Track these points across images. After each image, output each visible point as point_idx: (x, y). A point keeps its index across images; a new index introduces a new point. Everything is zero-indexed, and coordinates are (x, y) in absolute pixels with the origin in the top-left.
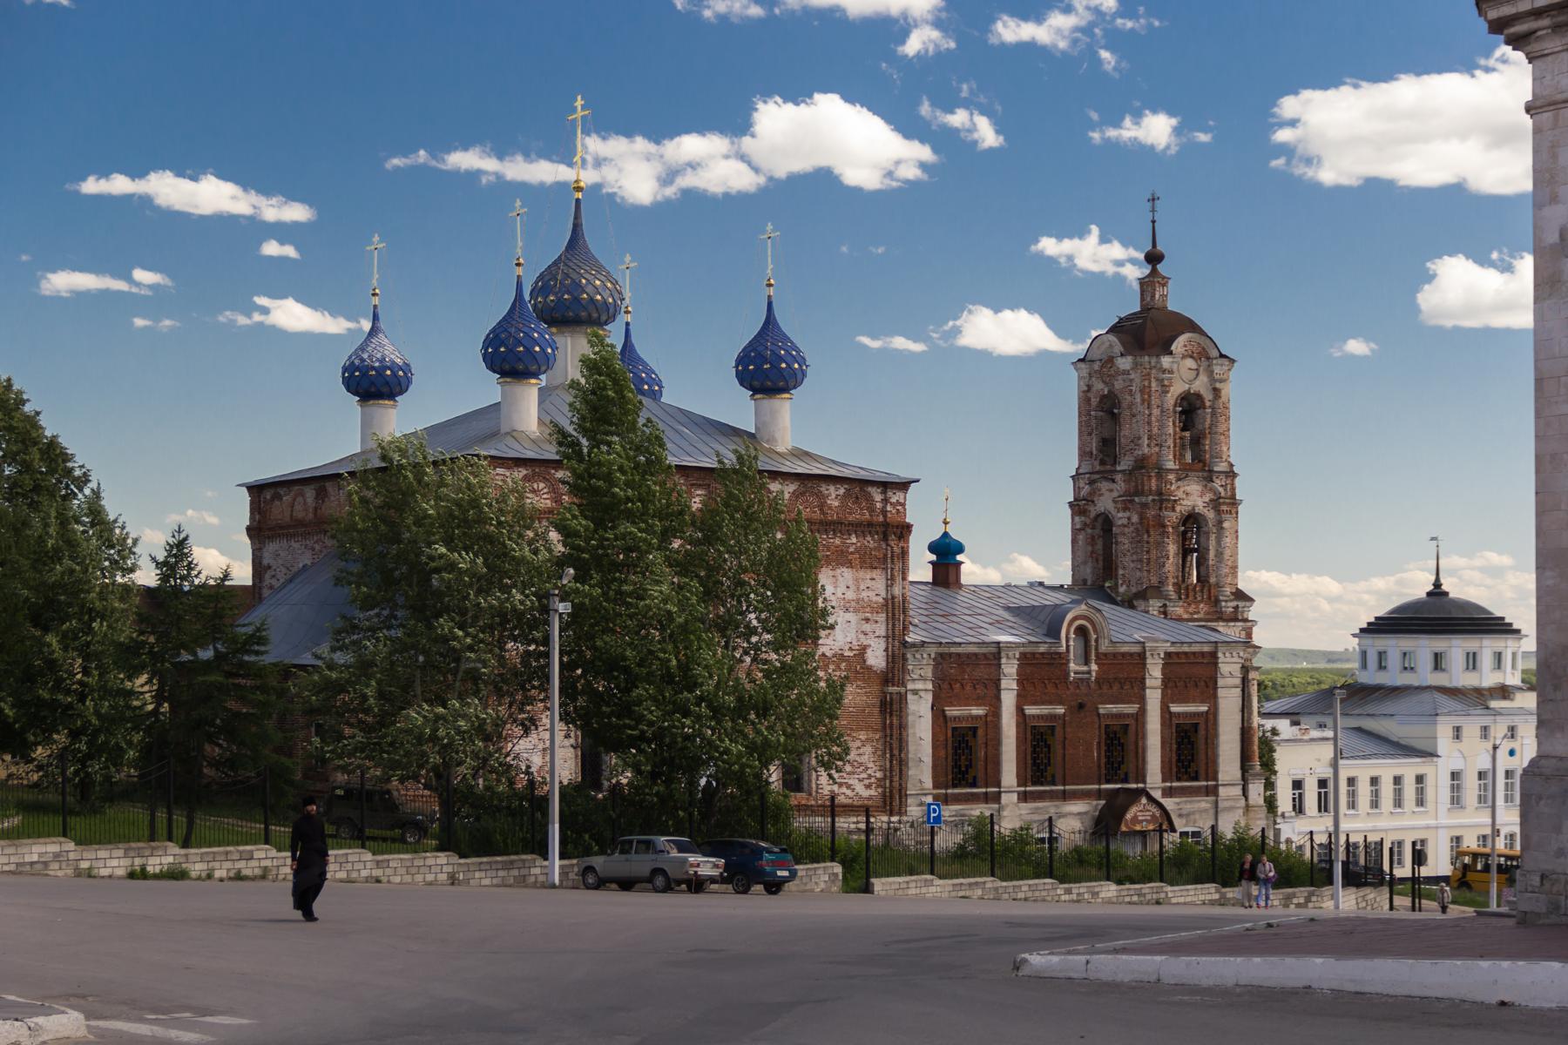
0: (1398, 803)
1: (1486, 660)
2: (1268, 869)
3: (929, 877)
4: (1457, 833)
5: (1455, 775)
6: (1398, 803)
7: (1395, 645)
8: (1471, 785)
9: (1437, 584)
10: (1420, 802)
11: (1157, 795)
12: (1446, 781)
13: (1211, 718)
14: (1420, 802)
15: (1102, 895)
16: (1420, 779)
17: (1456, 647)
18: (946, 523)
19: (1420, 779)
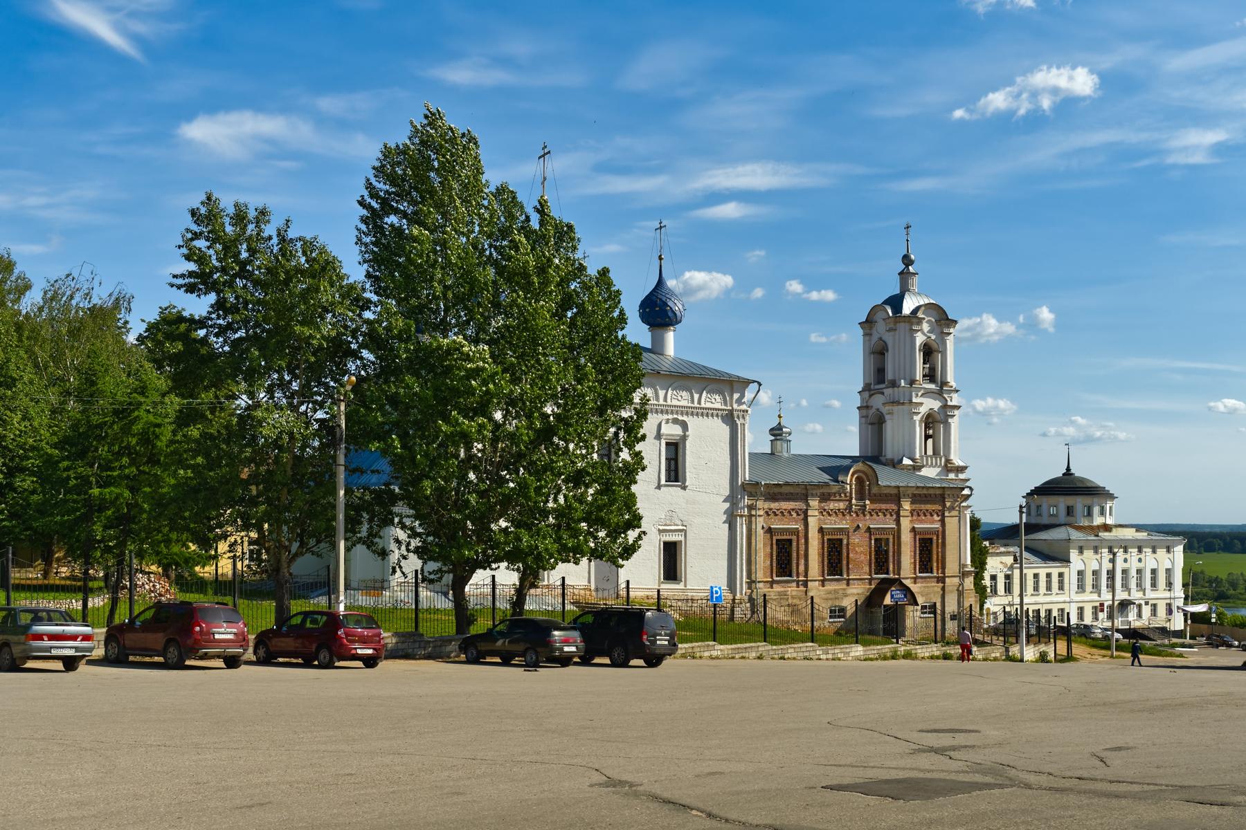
0: (1049, 588)
1: (1096, 510)
2: (567, 641)
3: (711, 643)
4: (1081, 605)
5: (1080, 573)
6: (1049, 588)
7: (1045, 501)
8: (1055, 584)
9: (1068, 469)
10: (1061, 588)
11: (907, 582)
12: (1074, 577)
14: (1061, 588)
15: (852, 654)
16: (1061, 575)
17: (1079, 502)
19: (1061, 575)
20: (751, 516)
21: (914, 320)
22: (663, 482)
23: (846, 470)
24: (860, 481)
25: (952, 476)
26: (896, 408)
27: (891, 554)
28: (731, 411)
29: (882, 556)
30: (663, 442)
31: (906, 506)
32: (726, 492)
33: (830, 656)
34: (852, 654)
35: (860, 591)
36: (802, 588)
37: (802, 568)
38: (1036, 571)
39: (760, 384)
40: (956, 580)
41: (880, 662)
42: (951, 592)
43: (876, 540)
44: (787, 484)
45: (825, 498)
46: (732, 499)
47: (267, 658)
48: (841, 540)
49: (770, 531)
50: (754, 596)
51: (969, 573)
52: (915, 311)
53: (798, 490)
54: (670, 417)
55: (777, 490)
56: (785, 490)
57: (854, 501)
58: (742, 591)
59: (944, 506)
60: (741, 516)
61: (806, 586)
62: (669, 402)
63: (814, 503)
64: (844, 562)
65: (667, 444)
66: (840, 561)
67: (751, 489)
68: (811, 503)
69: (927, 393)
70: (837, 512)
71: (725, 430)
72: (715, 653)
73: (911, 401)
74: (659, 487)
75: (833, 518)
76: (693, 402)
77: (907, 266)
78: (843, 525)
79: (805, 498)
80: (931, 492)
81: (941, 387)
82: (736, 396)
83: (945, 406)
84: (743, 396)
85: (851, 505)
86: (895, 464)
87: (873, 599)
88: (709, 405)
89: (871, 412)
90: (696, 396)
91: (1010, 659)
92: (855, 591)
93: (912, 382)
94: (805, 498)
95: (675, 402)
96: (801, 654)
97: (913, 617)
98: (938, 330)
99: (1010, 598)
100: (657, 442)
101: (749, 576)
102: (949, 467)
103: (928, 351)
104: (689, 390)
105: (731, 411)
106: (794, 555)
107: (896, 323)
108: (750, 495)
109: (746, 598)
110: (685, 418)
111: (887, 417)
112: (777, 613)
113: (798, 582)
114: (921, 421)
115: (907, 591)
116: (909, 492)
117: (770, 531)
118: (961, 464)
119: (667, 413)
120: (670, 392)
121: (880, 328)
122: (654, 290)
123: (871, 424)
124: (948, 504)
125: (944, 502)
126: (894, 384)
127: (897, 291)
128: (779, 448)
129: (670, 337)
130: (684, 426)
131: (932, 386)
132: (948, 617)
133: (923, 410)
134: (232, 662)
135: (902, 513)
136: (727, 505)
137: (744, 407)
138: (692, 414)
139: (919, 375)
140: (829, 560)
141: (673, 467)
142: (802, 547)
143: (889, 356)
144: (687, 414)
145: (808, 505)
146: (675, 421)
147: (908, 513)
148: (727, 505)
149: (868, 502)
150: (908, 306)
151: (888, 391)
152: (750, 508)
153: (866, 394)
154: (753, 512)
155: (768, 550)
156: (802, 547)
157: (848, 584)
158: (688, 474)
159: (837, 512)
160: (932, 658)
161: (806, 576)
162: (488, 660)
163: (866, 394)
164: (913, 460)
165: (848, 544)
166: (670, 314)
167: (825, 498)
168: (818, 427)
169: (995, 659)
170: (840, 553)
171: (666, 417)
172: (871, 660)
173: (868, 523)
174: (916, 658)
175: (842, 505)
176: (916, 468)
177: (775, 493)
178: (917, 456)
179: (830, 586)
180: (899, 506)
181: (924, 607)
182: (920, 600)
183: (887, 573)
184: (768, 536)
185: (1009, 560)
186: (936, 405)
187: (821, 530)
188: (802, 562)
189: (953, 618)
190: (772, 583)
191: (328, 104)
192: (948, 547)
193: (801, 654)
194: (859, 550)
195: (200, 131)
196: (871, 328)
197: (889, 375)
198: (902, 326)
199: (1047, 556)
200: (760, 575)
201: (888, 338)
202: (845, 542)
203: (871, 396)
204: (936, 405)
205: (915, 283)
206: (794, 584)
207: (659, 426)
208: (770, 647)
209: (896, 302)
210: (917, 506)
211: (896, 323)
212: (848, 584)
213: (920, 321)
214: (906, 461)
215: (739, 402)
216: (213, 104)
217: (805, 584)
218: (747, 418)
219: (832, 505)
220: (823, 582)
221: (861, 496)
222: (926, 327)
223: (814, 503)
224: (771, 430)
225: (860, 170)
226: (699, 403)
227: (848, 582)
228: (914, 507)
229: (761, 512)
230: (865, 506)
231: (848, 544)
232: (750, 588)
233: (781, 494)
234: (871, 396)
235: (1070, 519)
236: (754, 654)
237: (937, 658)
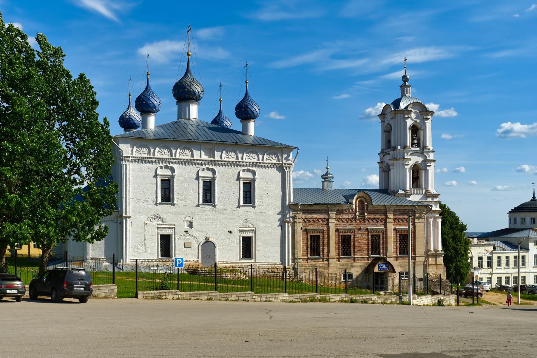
0: (507, 264)
7: (519, 216)
9: (534, 197)
16: (523, 257)
20: (294, 222)
21: (405, 112)
22: (241, 203)
23: (352, 196)
24: (361, 203)
25: (429, 200)
26: (395, 162)
27: (381, 243)
28: (282, 165)
29: (376, 243)
30: (241, 182)
31: (391, 216)
32: (279, 209)
33: (264, 300)
34: (281, 298)
35: (362, 264)
36: (326, 262)
37: (326, 251)
38: (507, 255)
39: (298, 149)
40: (423, 259)
41: (300, 304)
42: (420, 265)
43: (372, 236)
44: (316, 204)
45: (339, 212)
46: (283, 213)
47: (33, 298)
48: (350, 236)
49: (306, 231)
50: (296, 267)
51: (440, 255)
52: (406, 107)
53: (323, 208)
54: (245, 168)
55: (310, 208)
56: (314, 208)
57: (357, 214)
58: (289, 263)
59: (415, 216)
60: (288, 222)
61: (328, 261)
62: (244, 160)
63: (333, 215)
64: (352, 248)
65: (244, 183)
66: (350, 247)
67: (294, 207)
68: (331, 215)
69: (414, 153)
70: (347, 220)
71: (279, 175)
72: (176, 296)
73: (404, 158)
74: (239, 207)
75: (345, 223)
76: (259, 160)
77: (405, 82)
78: (352, 227)
79: (327, 212)
80: (406, 208)
81: (423, 150)
82: (285, 156)
83: (425, 160)
84: (289, 156)
85: (356, 216)
86: (394, 193)
87: (368, 270)
88: (268, 161)
89: (384, 164)
90: (261, 157)
91: (402, 303)
92: (359, 264)
93: (405, 147)
94: (327, 212)
95: (248, 160)
96: (242, 298)
97: (394, 280)
98: (421, 117)
99: (491, 270)
100: (238, 182)
101: (293, 254)
102: (428, 195)
103: (415, 129)
104: (235, 152)
105: (282, 165)
106: (321, 244)
107: (395, 114)
108: (294, 211)
109: (292, 268)
110: (254, 169)
111: (391, 167)
112: (307, 276)
113: (323, 259)
114: (410, 169)
115: (389, 264)
116: (393, 208)
117: (306, 231)
118: (435, 193)
119: (243, 166)
120: (266, 155)
121: (389, 116)
122: (242, 100)
123: (384, 171)
124: (417, 215)
125: (415, 214)
126: (395, 148)
127: (400, 97)
128: (326, 185)
129: (252, 125)
130: (254, 173)
131: (418, 149)
132: (417, 279)
133: (411, 163)
134: (18, 298)
135: (388, 220)
136: (280, 216)
137: (289, 162)
138: (259, 166)
139: (409, 142)
140: (372, 246)
141: (248, 196)
142: (326, 240)
143: (392, 133)
144: (255, 166)
145: (329, 216)
146: (248, 171)
147: (392, 220)
148: (280, 216)
149: (366, 214)
150: (402, 106)
151: (391, 153)
152: (294, 218)
153: (382, 155)
154: (296, 220)
155: (305, 241)
156: (326, 240)
157: (354, 260)
158: (256, 200)
159: (347, 220)
160: (342, 301)
161: (328, 255)
162: (65, 299)
163: (382, 155)
164: (405, 191)
165: (354, 238)
166: (250, 112)
167: (339, 212)
168: (454, 182)
169: (391, 303)
170: (349, 243)
171: (243, 168)
172: (295, 302)
173: (366, 226)
174: (330, 302)
175: (350, 216)
176: (408, 195)
177: (308, 209)
178: (408, 188)
179: (344, 262)
180: (386, 216)
181: (401, 274)
182: (398, 270)
183: (379, 254)
184: (305, 233)
185: (491, 248)
186: (419, 160)
187: (337, 230)
188: (326, 248)
189: (420, 280)
190: (307, 260)
191: (204, 33)
192: (417, 240)
193: (242, 298)
194: (361, 241)
195: (146, 50)
196: (384, 118)
197: (392, 144)
198: (399, 116)
199: (513, 246)
200: (300, 255)
201: (392, 123)
202: (352, 236)
203: (384, 156)
204: (419, 160)
205: (409, 92)
206: (321, 260)
207: (239, 173)
208: (218, 293)
209: (397, 103)
210: (398, 216)
211: (395, 114)
212: (354, 260)
213: (409, 112)
214: (401, 192)
215: (287, 159)
216: (152, 38)
217: (328, 260)
218: (292, 168)
219: (344, 216)
220: (339, 259)
221: (362, 211)
222: (413, 116)
223: (333, 215)
224: (322, 176)
225: (471, 48)
226: (263, 160)
227: (354, 259)
228: (395, 217)
229: (301, 220)
230: (364, 216)
231: (354, 238)
232: (294, 262)
233: (312, 210)
234: (384, 156)
235: (533, 226)
236: (206, 297)
237: (346, 302)
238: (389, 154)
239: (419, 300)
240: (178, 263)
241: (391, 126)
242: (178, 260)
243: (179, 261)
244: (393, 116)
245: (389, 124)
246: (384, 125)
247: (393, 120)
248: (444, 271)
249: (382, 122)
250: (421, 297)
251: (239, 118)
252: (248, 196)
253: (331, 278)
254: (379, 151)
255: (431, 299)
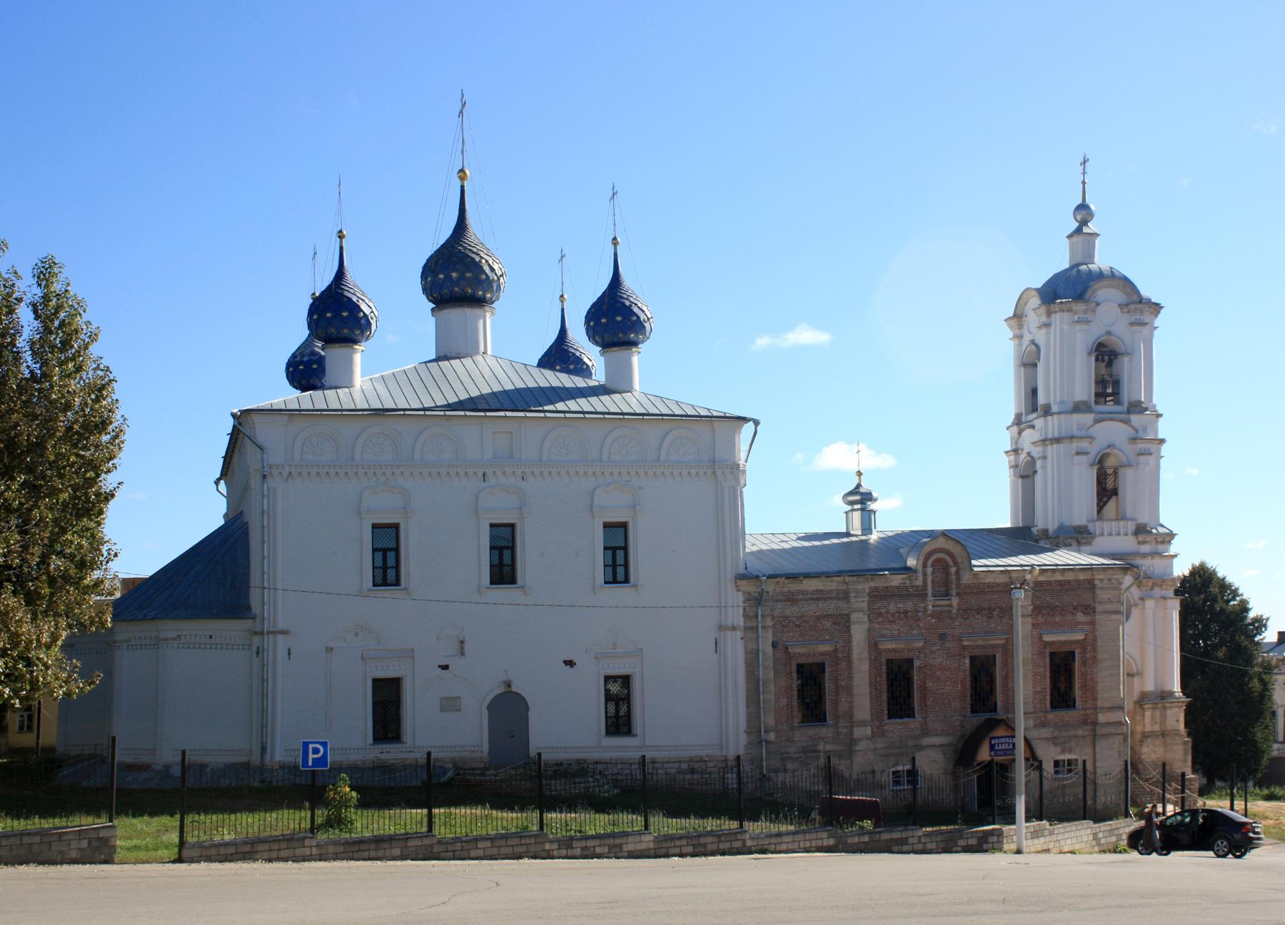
13: (1008, 649)
18: (859, 474)
64: (916, 695)
153: (1015, 429)
163: (1015, 429)
196: (1020, 326)
197: (1041, 400)
203: (1020, 433)
238: (1033, 427)
239: (1054, 838)
240: (311, 756)
241: (1037, 347)
242: (311, 746)
243: (316, 751)
244: (1044, 319)
245: (1033, 342)
246: (1020, 345)
247: (1044, 331)
248: (1186, 753)
249: (1019, 337)
250: (1060, 827)
251: (597, 343)
252: (620, 560)
253: (859, 785)
254: (1011, 418)
255: (1095, 835)
